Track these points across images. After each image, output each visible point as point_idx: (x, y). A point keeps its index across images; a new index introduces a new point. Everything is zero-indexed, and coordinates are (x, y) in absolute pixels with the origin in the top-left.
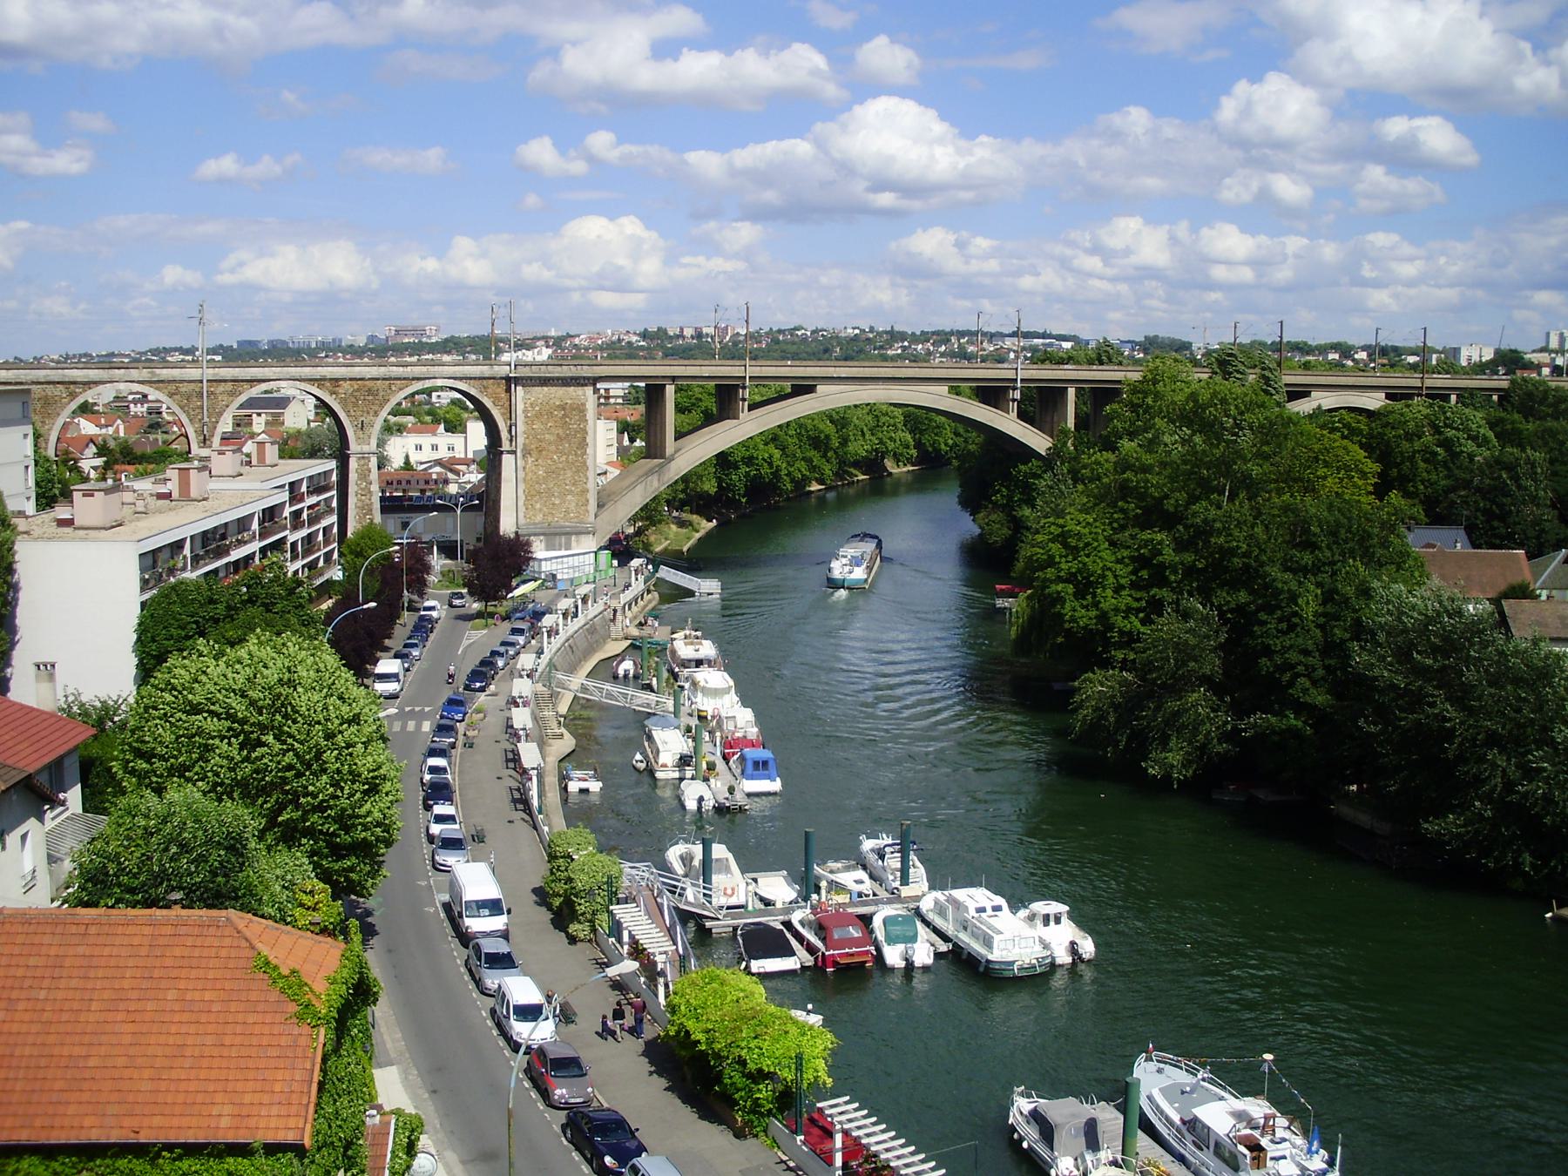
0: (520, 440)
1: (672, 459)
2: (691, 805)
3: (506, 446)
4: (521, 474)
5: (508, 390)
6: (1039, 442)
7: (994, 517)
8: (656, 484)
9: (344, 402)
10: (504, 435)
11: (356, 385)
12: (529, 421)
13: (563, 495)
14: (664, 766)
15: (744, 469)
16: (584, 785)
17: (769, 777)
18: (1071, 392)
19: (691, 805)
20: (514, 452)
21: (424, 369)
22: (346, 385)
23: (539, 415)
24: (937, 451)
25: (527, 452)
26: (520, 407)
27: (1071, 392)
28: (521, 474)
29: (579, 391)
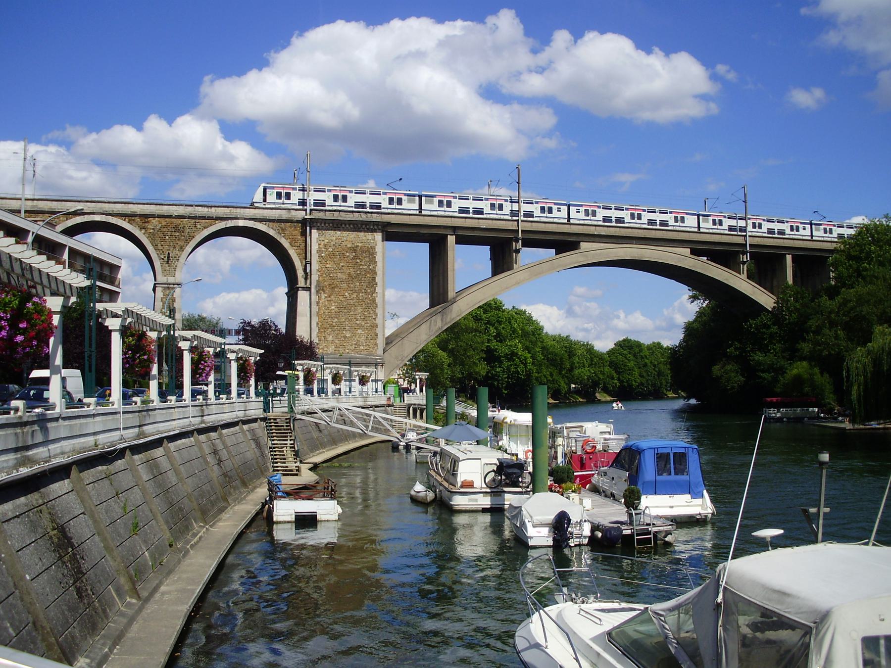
0: (315, 277)
1: (454, 301)
2: (539, 536)
3: (301, 283)
4: (315, 308)
5: (304, 234)
6: (766, 300)
7: (729, 367)
8: (439, 324)
9: (152, 237)
10: (300, 273)
11: (164, 222)
12: (322, 260)
13: (354, 329)
14: (469, 484)
15: (506, 364)
16: (305, 506)
17: (688, 489)
18: (789, 258)
19: (539, 536)
20: (308, 289)
21: (227, 210)
22: (155, 221)
23: (332, 256)
24: (630, 386)
25: (320, 289)
26: (315, 247)
27: (789, 258)
28: (315, 308)
29: (369, 236)
